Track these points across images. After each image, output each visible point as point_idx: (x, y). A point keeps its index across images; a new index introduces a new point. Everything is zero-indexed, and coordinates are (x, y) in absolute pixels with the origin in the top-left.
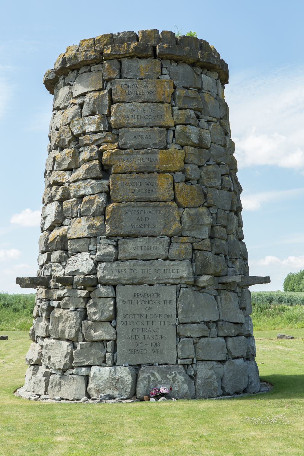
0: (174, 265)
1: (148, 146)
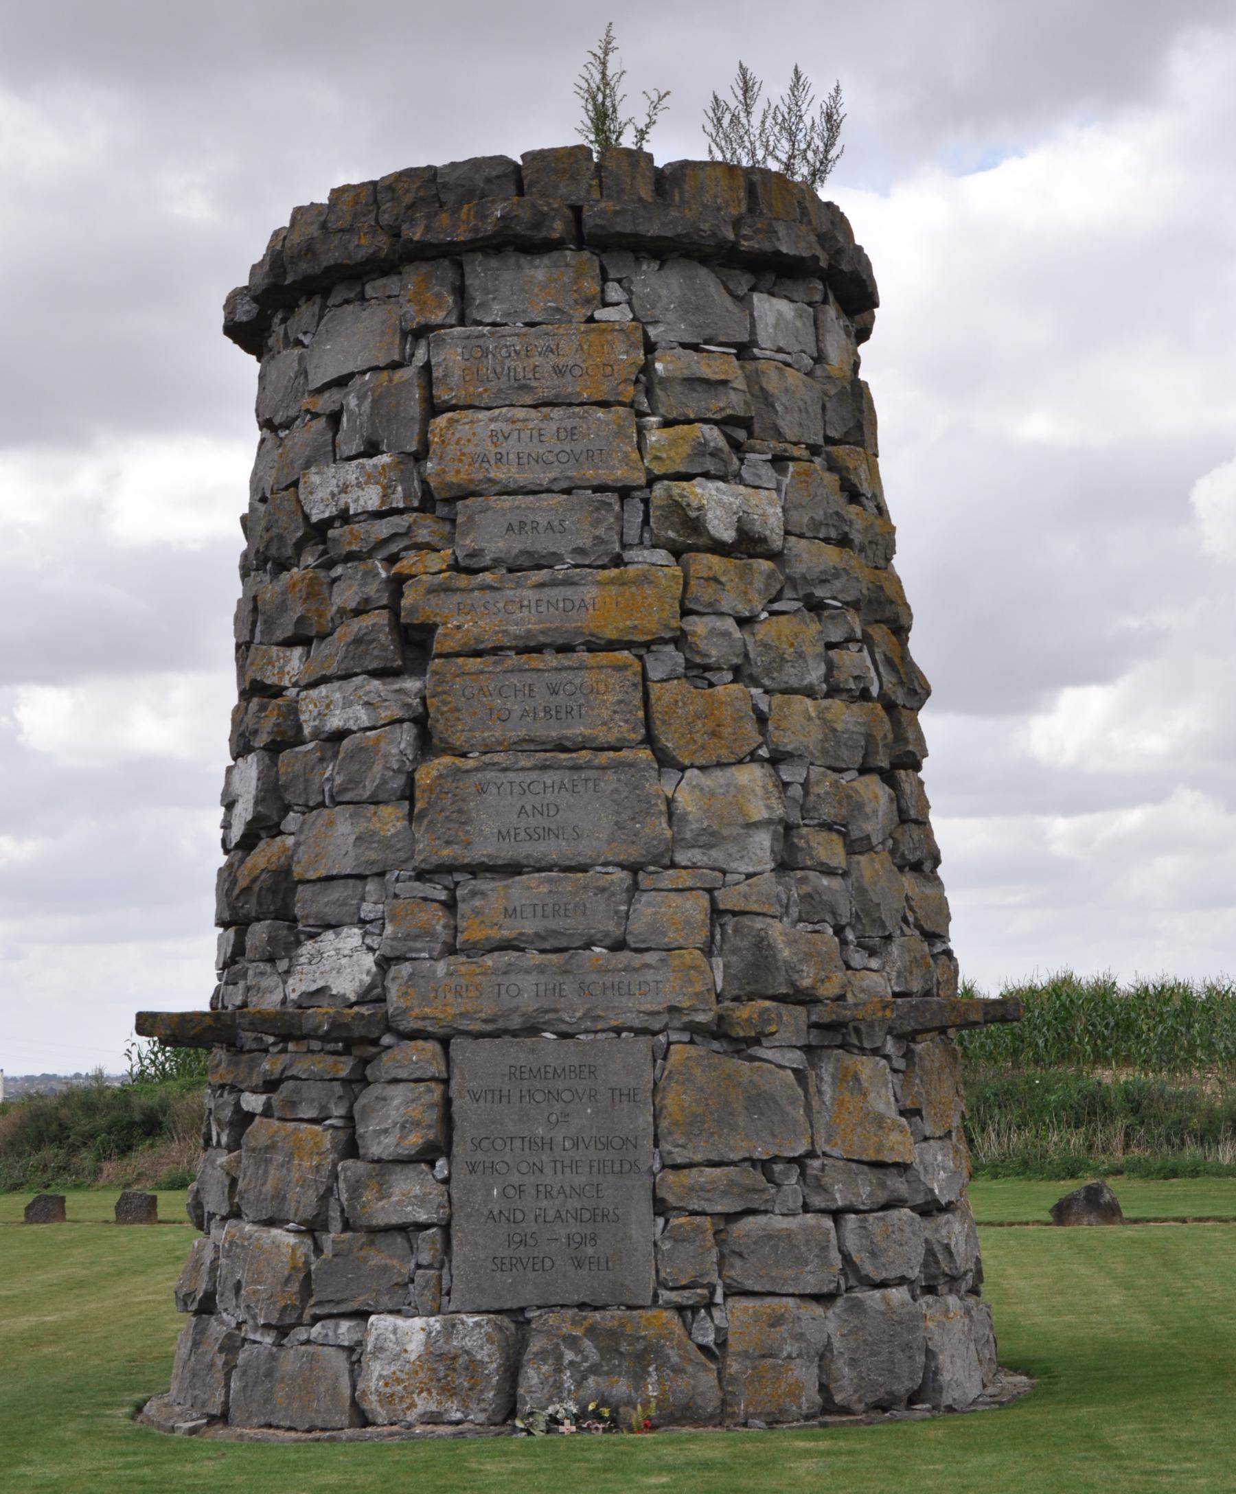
1: (557, 558)
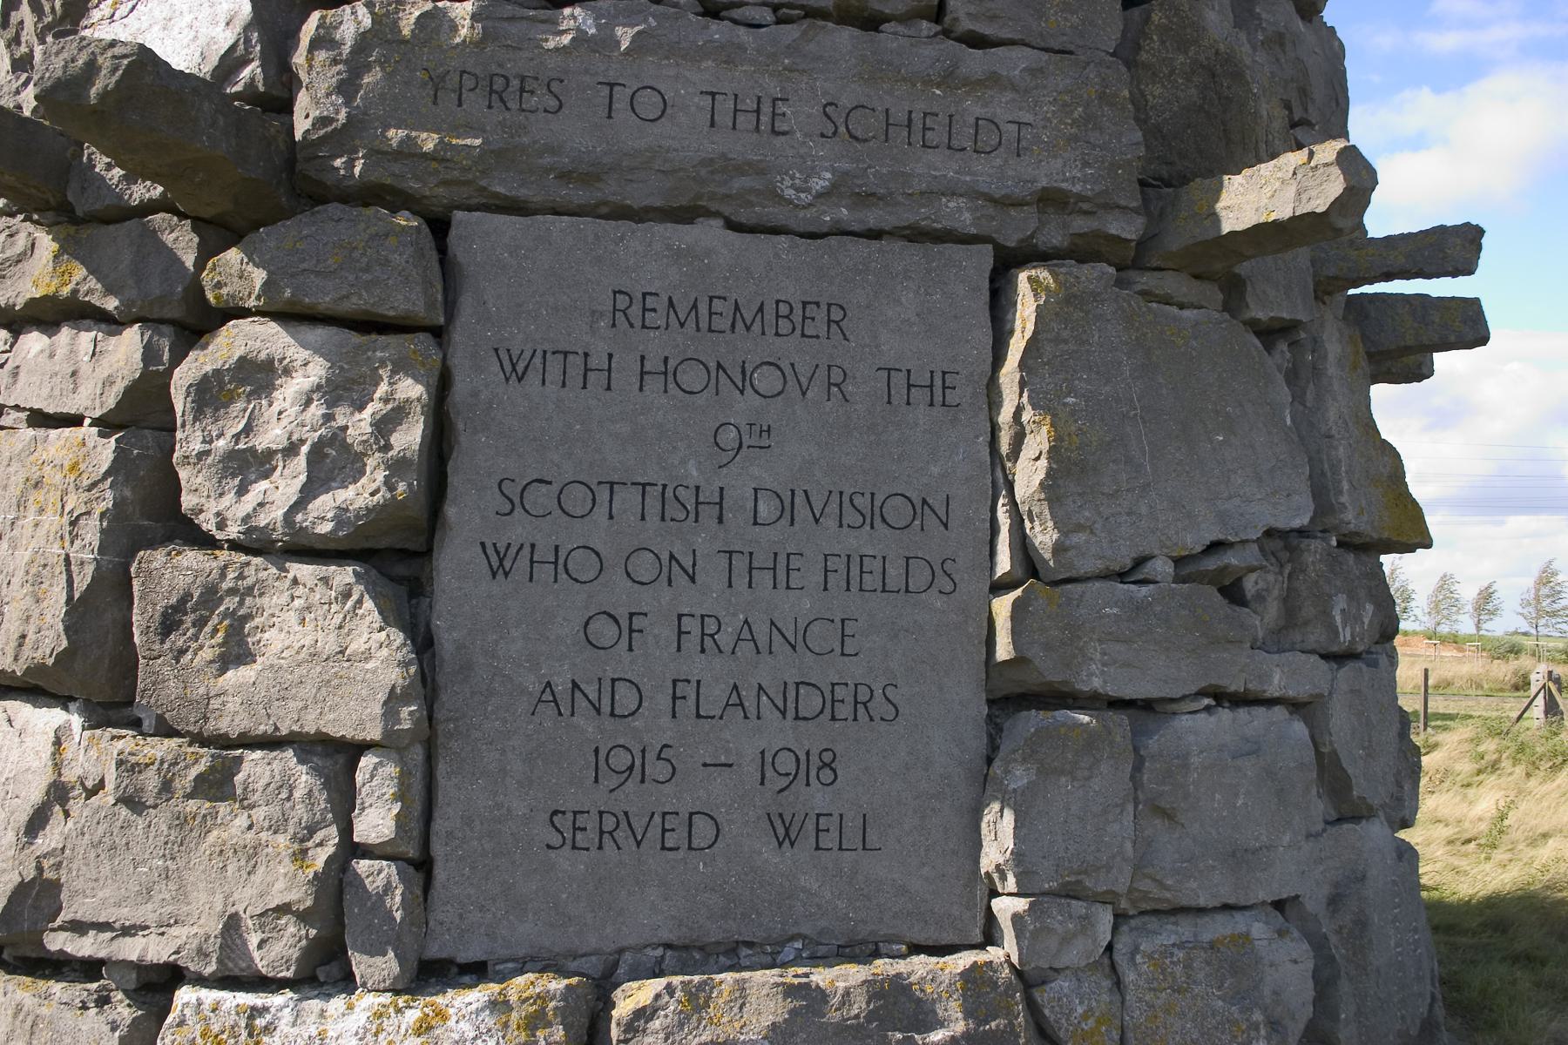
0: (993, 80)
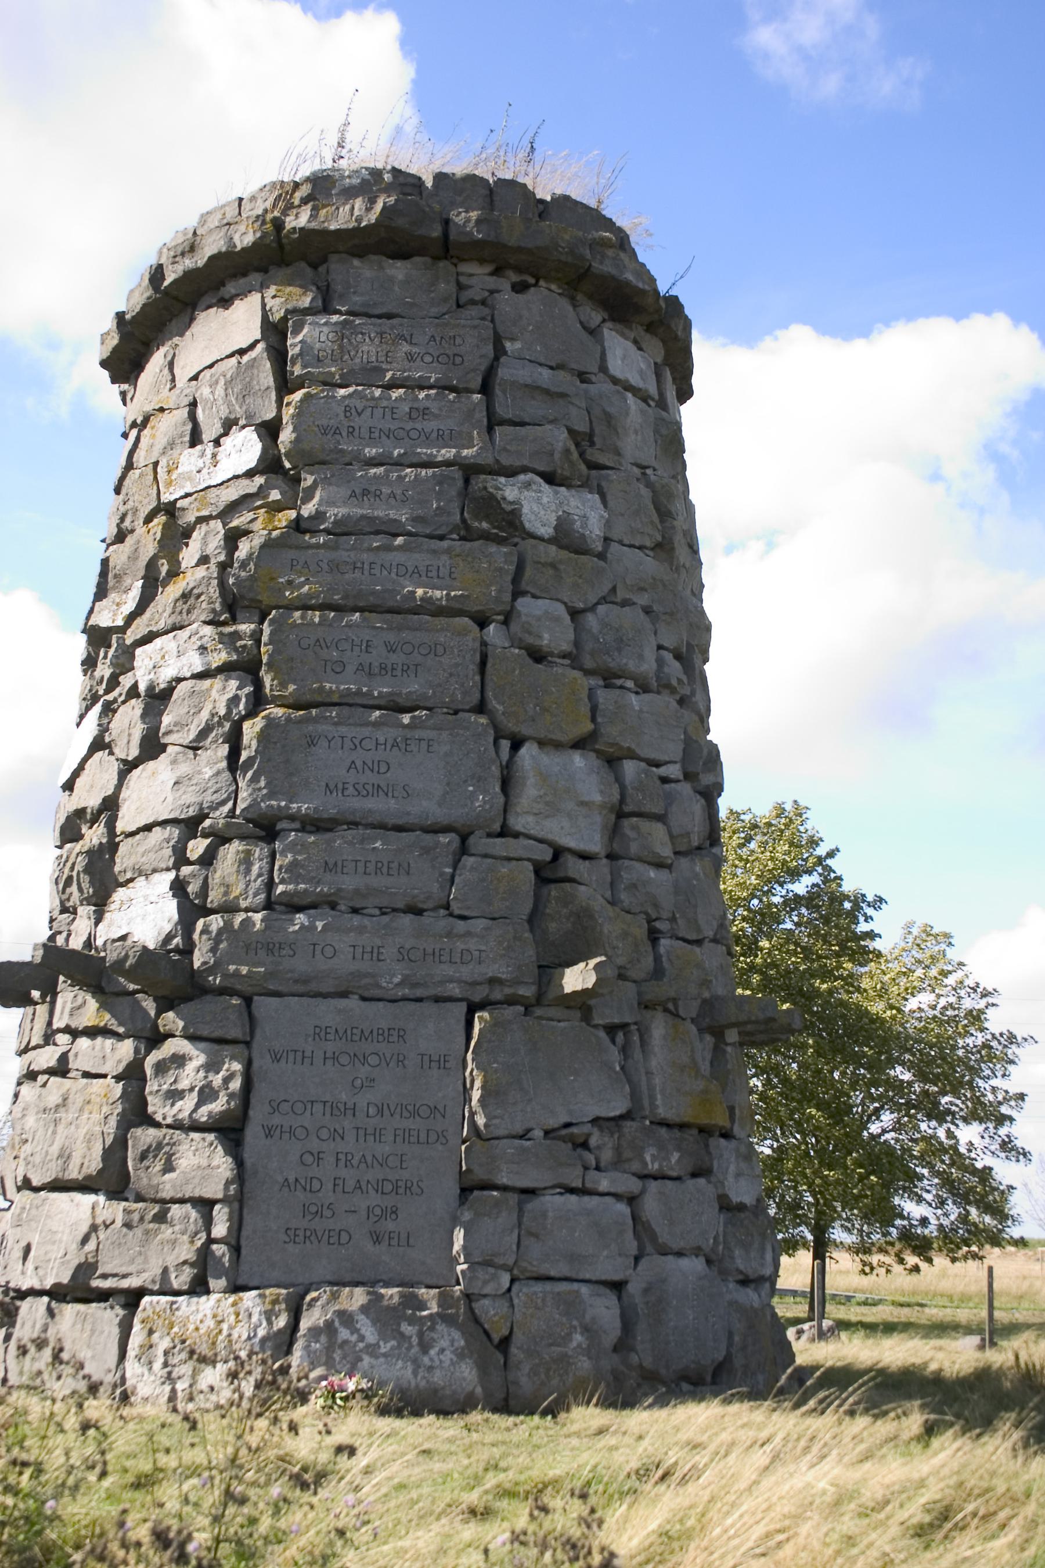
0: (468, 934)
